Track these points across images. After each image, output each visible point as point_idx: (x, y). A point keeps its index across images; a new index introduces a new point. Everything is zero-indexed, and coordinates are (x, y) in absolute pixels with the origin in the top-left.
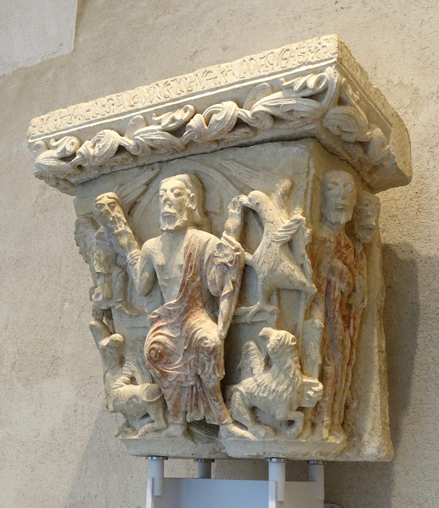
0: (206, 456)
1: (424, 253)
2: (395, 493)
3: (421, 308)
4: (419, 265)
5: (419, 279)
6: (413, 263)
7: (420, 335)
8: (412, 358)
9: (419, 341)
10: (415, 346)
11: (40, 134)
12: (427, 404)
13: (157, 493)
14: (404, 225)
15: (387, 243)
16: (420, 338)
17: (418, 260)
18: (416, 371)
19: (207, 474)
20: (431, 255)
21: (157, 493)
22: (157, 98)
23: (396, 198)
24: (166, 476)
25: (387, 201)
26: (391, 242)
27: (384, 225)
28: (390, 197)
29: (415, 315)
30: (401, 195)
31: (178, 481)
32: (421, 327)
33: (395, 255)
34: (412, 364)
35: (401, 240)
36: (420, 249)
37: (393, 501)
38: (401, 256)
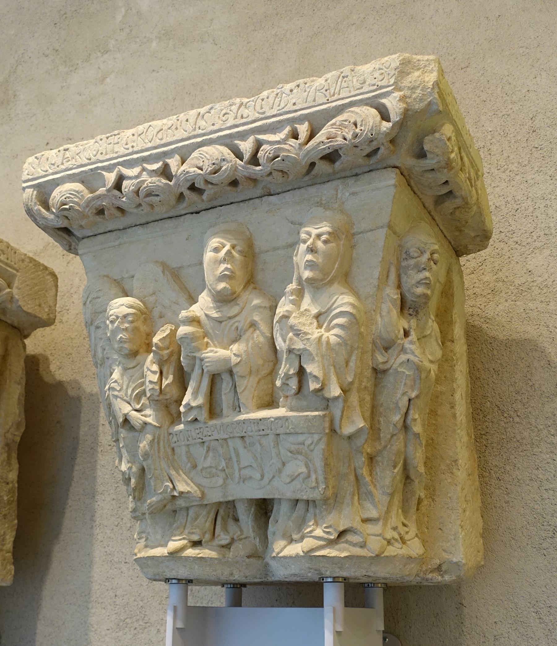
0: (238, 577)
1: (88, 390)
2: (41, 617)
3: (80, 442)
4: (84, 401)
5: (82, 415)
6: (79, 399)
7: (77, 468)
8: (68, 490)
9: (75, 473)
10: (71, 478)
11: (45, 173)
12: (75, 533)
13: (180, 625)
14: (76, 363)
15: (61, 380)
16: (76, 471)
17: (83, 397)
18: (70, 502)
19: (236, 602)
20: (93, 392)
21: (180, 625)
22: (183, 131)
23: (73, 337)
24: (189, 604)
25: (66, 339)
26: (64, 379)
27: (61, 363)
28: (68, 335)
29: (75, 449)
30: (77, 334)
31: (204, 610)
32: (78, 461)
33: (66, 392)
34: (68, 495)
35: (72, 378)
36: (86, 387)
37: (38, 625)
38: (71, 393)
